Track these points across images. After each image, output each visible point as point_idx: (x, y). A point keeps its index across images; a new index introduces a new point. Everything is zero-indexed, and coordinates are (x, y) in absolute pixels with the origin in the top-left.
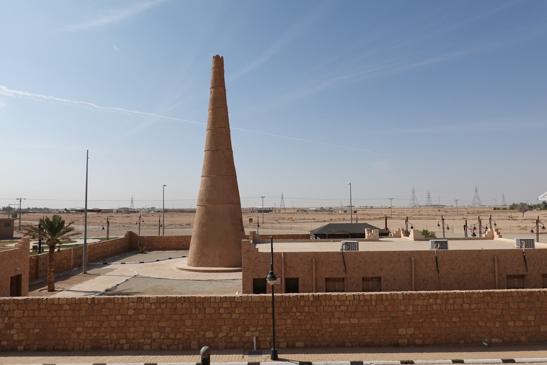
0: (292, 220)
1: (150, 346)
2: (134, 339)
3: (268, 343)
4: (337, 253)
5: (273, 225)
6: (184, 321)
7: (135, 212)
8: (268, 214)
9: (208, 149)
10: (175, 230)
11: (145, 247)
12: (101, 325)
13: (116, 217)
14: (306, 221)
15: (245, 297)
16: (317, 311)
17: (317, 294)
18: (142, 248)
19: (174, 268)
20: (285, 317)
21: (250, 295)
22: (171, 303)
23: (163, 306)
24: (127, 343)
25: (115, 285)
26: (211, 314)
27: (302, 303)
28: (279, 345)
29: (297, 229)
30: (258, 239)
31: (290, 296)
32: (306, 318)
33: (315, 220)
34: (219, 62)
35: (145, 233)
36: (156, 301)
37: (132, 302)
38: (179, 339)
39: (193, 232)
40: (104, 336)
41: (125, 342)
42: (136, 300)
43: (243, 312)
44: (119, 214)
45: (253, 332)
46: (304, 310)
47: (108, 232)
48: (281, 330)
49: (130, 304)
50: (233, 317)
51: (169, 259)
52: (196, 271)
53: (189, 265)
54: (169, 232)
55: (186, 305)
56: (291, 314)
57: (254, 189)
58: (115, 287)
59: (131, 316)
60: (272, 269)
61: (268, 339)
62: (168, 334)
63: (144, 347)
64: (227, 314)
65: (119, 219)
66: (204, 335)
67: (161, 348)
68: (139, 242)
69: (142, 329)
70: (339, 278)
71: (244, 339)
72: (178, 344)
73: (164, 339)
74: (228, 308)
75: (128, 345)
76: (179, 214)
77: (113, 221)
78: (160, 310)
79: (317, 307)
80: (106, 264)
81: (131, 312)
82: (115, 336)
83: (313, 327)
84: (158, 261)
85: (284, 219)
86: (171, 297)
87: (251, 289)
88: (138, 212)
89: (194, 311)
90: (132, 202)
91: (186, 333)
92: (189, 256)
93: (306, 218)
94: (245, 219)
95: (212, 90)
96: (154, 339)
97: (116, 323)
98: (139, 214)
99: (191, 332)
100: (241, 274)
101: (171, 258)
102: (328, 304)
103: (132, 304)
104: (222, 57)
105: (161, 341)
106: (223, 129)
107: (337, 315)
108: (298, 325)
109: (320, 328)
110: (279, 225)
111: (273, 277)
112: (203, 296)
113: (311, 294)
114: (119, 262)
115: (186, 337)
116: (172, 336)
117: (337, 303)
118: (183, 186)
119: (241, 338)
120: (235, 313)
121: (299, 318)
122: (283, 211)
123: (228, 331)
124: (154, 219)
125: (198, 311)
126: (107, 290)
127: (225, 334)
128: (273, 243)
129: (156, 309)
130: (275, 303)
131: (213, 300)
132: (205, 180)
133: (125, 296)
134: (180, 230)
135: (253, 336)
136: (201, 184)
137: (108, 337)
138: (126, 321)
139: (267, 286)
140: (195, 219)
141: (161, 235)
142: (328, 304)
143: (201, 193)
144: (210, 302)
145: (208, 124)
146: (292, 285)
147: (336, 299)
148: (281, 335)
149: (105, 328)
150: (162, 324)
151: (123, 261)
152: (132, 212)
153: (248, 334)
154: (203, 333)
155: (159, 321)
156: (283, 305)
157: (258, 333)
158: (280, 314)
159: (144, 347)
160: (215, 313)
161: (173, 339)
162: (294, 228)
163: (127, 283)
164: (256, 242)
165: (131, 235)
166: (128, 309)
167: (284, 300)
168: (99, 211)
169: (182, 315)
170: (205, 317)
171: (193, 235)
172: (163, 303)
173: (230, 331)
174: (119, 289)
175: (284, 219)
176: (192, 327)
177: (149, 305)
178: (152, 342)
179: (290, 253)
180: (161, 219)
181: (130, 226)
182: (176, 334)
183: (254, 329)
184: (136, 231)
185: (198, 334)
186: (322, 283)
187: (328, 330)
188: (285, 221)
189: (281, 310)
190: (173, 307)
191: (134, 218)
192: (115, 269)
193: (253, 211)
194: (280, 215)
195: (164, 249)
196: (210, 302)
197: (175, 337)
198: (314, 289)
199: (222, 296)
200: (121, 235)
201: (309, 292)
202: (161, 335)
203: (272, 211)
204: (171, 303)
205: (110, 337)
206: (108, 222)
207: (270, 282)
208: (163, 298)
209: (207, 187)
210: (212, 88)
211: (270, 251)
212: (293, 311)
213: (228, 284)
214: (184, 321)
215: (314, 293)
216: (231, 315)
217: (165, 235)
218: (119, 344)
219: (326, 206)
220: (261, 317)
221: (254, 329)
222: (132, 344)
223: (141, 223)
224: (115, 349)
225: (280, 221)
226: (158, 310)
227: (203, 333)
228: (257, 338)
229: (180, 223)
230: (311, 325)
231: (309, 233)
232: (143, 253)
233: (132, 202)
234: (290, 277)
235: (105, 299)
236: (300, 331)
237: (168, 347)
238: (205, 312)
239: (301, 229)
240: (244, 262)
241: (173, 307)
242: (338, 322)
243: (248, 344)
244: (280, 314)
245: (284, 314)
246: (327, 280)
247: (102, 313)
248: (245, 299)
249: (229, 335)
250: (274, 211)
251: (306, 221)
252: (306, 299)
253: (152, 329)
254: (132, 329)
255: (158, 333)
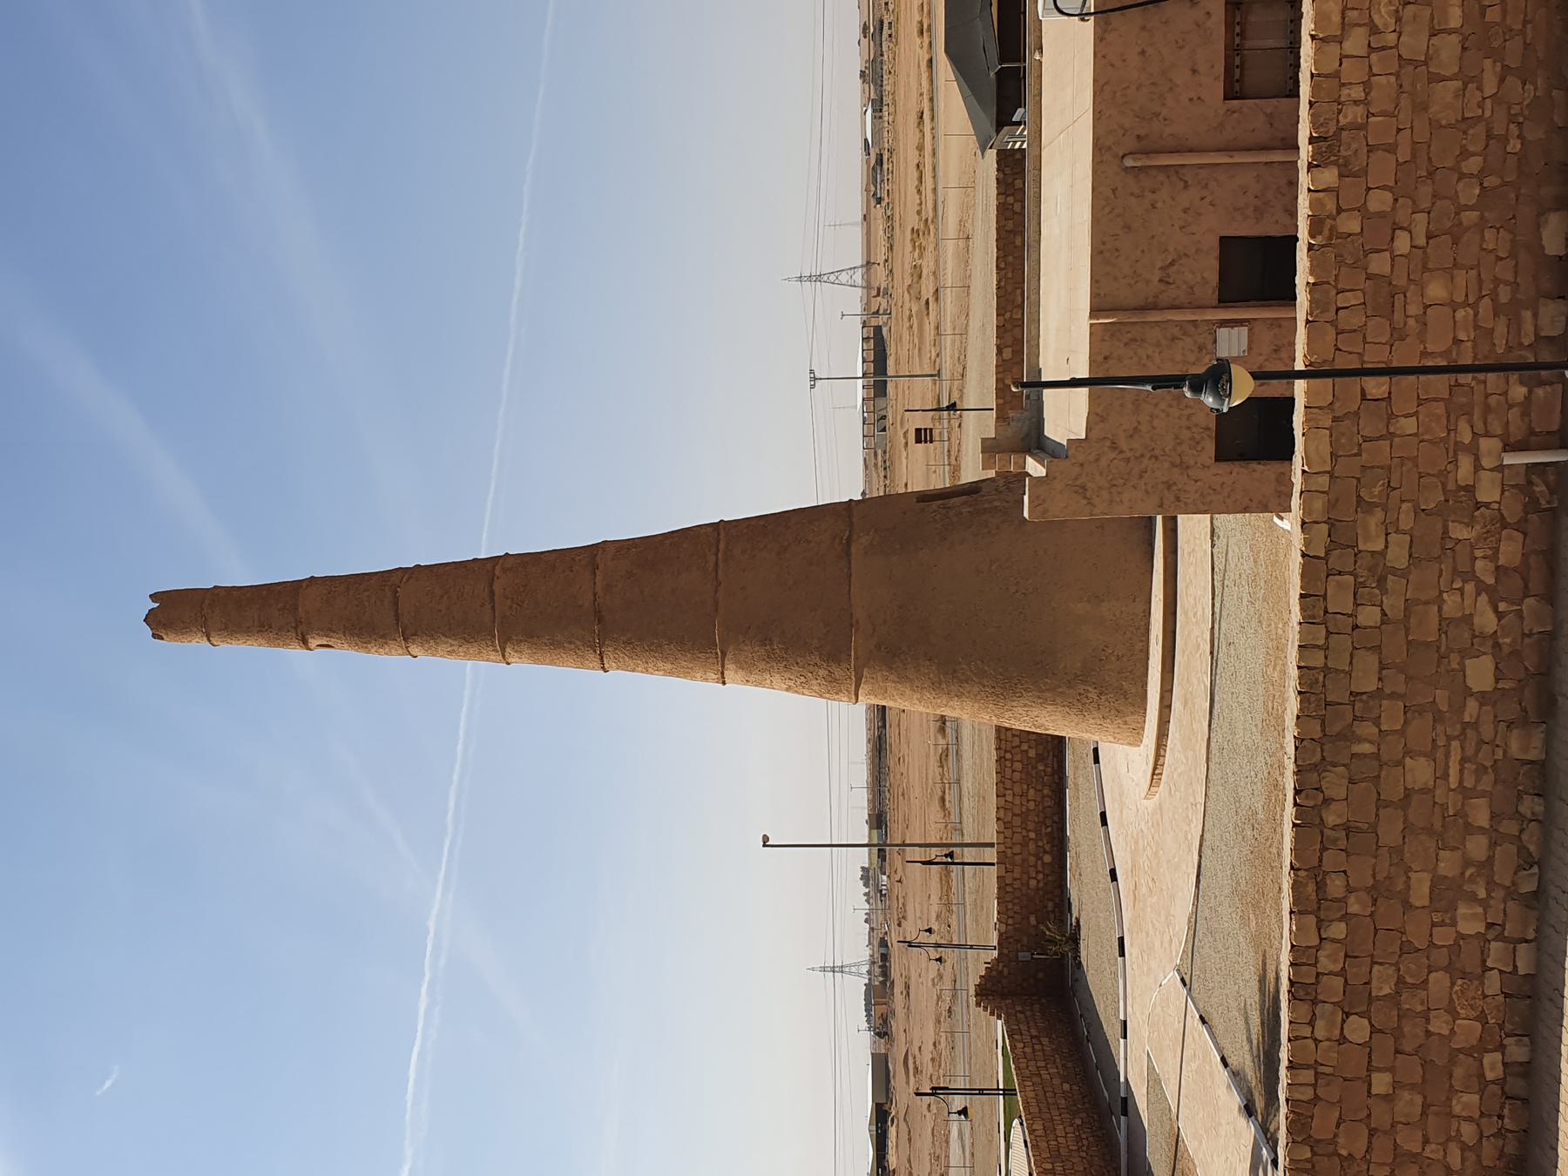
0: (927, 227)
1: (1522, 948)
2: (1482, 1018)
3: (1540, 392)
4: (1099, 39)
5: (947, 327)
6: (1408, 793)
7: (885, 957)
8: (891, 350)
9: (593, 658)
10: (968, 784)
11: (1050, 930)
12: (1414, 1157)
13: (909, 1042)
14: (928, 160)
15: (1307, 508)
16: (1391, 149)
17: (1305, 151)
18: (1052, 941)
19: (1151, 804)
20: (1413, 309)
21: (1297, 479)
22: (1324, 849)
23: (1335, 886)
24: (1502, 1048)
25: (1224, 1074)
26: (1382, 667)
27: (1351, 224)
28: (1550, 339)
29: (966, 208)
30: (1021, 429)
31: (1312, 287)
32: (1426, 205)
33: (926, 116)
34: (178, 613)
35: (981, 921)
36: (1311, 920)
37: (1312, 1023)
38: (1493, 816)
39: (978, 721)
40: (1464, 1148)
41: (1498, 1056)
42: (1304, 1008)
43: (1379, 514)
44: (897, 1026)
45: (1478, 467)
46: (1381, 215)
47: (981, 1092)
48: (1477, 327)
49: (1319, 1034)
50: (1402, 563)
51: (1104, 822)
52: (1164, 722)
53: (1136, 739)
54: (980, 818)
55: (1334, 782)
56: (1400, 280)
57: (780, 441)
58: (1236, 1075)
59: (1374, 1030)
60: (1174, 382)
61: (1518, 392)
62: (1467, 863)
63: (1521, 972)
64: (1384, 592)
65: (919, 1030)
66: (1483, 698)
67: (1535, 894)
68: (1024, 956)
69: (1439, 981)
70: (1229, 25)
71: (1513, 511)
72: (1521, 817)
73: (1491, 884)
74: (1358, 585)
75: (1507, 1041)
76: (891, 761)
77: (927, 1056)
78: (1352, 899)
79: (1371, 149)
80: (1126, 1105)
81: (1358, 1029)
82: (1466, 1098)
83: (1473, 165)
84: (1113, 873)
85: (917, 272)
86: (1297, 850)
87: (1265, 471)
88: (883, 943)
89: (1366, 748)
90: (842, 970)
91: (1469, 782)
92: (1096, 738)
93: (913, 157)
94: (919, 472)
95: (313, 642)
96: (1490, 926)
97: (1406, 1095)
98: (895, 949)
99: (1463, 760)
100: (1193, 528)
101: (1103, 815)
102: (1357, 93)
103: (1320, 1024)
104: (154, 597)
105: (1499, 894)
106: (497, 587)
107: (1414, 43)
108: (1455, 243)
109: (1479, 130)
110: (948, 297)
111: (1217, 377)
112: (1293, 705)
113: (1304, 180)
114: (1119, 1049)
115: (1486, 783)
116: (1477, 847)
117: (1355, 43)
118: (770, 760)
119: (1505, 526)
120: (1383, 553)
121: (1421, 241)
122: (880, 275)
123: (1470, 588)
124: (921, 891)
125: (1368, 729)
126: (1249, 1110)
127: (1484, 598)
128: (1046, 377)
129: (1346, 917)
130: (1340, 364)
131: (1318, 660)
132: (741, 666)
133: (1284, 1055)
134: (967, 763)
135: (1501, 468)
136: (758, 684)
137: (1468, 1131)
138: (1397, 1052)
139: (1258, 395)
140: (915, 708)
141: (991, 855)
142: (1357, 93)
143: (801, 686)
144: (1326, 670)
145: (478, 656)
146: (1256, 271)
147: (1333, 48)
148: (1501, 328)
149: (1426, 1141)
150: (1420, 893)
151: (1111, 1031)
152: (885, 972)
153: (1488, 492)
154: (1472, 706)
155: (1407, 906)
156: (1353, 320)
157: (1485, 444)
158: (1398, 334)
159: (1521, 972)
160: (1377, 649)
161: (1493, 844)
162: (962, 223)
163: (1215, 1020)
164: (1035, 442)
165: (992, 991)
166: (1343, 1039)
167: (1331, 315)
168: (881, 1116)
169: (1381, 803)
170: (1393, 696)
171: (995, 721)
172: (1320, 886)
173: (1470, 575)
174: (1244, 1058)
175: (917, 272)
176: (1440, 755)
177: (1328, 948)
178: (1500, 938)
179: (1095, 281)
180: (917, 854)
181: (948, 984)
182: (1469, 829)
183: (1466, 463)
184: (976, 966)
185: (1475, 725)
186: (1253, 115)
187: (1490, 89)
188: (928, 266)
189: (1378, 330)
190: (1343, 844)
191: (915, 968)
192: (1151, 1068)
193: (877, 422)
194: (899, 291)
195: (1059, 843)
196: (1326, 670)
197: (1481, 830)
198: (1277, 157)
199: (1296, 615)
200: (990, 1030)
201: (1293, 184)
202: (1473, 898)
203: (878, 329)
204: (1324, 849)
205: (1469, 1119)
206: (935, 1091)
207: (1243, 388)
208: (1295, 887)
209: (770, 657)
210: (305, 643)
211: (1084, 391)
212: (1386, 270)
213: (1234, 587)
214: (1408, 793)
215: (1302, 164)
216: (1394, 571)
217: (991, 834)
218: (1501, 1082)
219: (851, 56)
220: (1409, 425)
221: (1466, 463)
222: (1508, 1027)
223: (933, 939)
224: (1525, 1101)
225: (927, 291)
226: (1354, 908)
227: (1472, 706)
228: (1508, 447)
229: (933, 762)
230: (1462, 176)
231: (992, 154)
232: (1075, 939)
233: (842, 970)
234: (1213, 277)
235: (1293, 1143)
236: (1488, 234)
237: (1527, 861)
238: (1371, 695)
239: (968, 188)
240: (1130, 505)
241: (1343, 844)
242: (1455, 38)
243: (1540, 488)
244: (1398, 334)
245: (1398, 316)
246: (1234, 90)
247: (1359, 1155)
248: (1319, 503)
249: (1491, 580)
250: (881, 320)
251: (928, 160)
252: (1331, 206)
253: (1443, 937)
254: (1439, 1025)
255: (1462, 910)
